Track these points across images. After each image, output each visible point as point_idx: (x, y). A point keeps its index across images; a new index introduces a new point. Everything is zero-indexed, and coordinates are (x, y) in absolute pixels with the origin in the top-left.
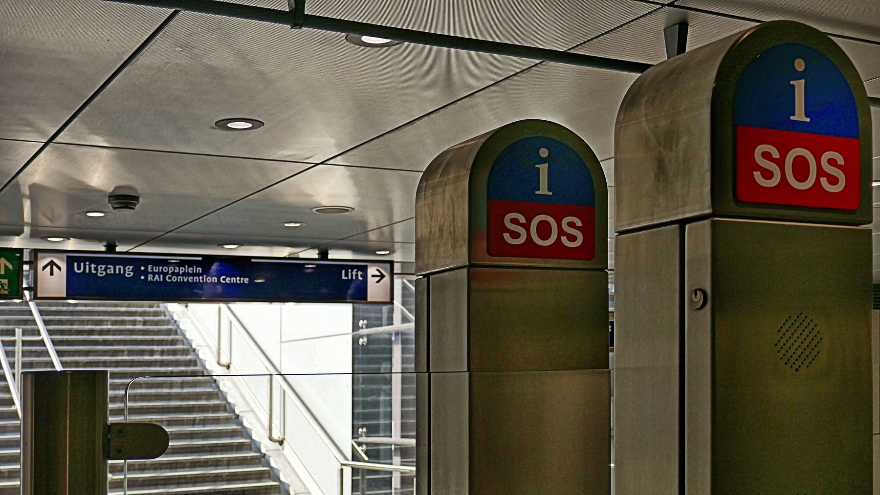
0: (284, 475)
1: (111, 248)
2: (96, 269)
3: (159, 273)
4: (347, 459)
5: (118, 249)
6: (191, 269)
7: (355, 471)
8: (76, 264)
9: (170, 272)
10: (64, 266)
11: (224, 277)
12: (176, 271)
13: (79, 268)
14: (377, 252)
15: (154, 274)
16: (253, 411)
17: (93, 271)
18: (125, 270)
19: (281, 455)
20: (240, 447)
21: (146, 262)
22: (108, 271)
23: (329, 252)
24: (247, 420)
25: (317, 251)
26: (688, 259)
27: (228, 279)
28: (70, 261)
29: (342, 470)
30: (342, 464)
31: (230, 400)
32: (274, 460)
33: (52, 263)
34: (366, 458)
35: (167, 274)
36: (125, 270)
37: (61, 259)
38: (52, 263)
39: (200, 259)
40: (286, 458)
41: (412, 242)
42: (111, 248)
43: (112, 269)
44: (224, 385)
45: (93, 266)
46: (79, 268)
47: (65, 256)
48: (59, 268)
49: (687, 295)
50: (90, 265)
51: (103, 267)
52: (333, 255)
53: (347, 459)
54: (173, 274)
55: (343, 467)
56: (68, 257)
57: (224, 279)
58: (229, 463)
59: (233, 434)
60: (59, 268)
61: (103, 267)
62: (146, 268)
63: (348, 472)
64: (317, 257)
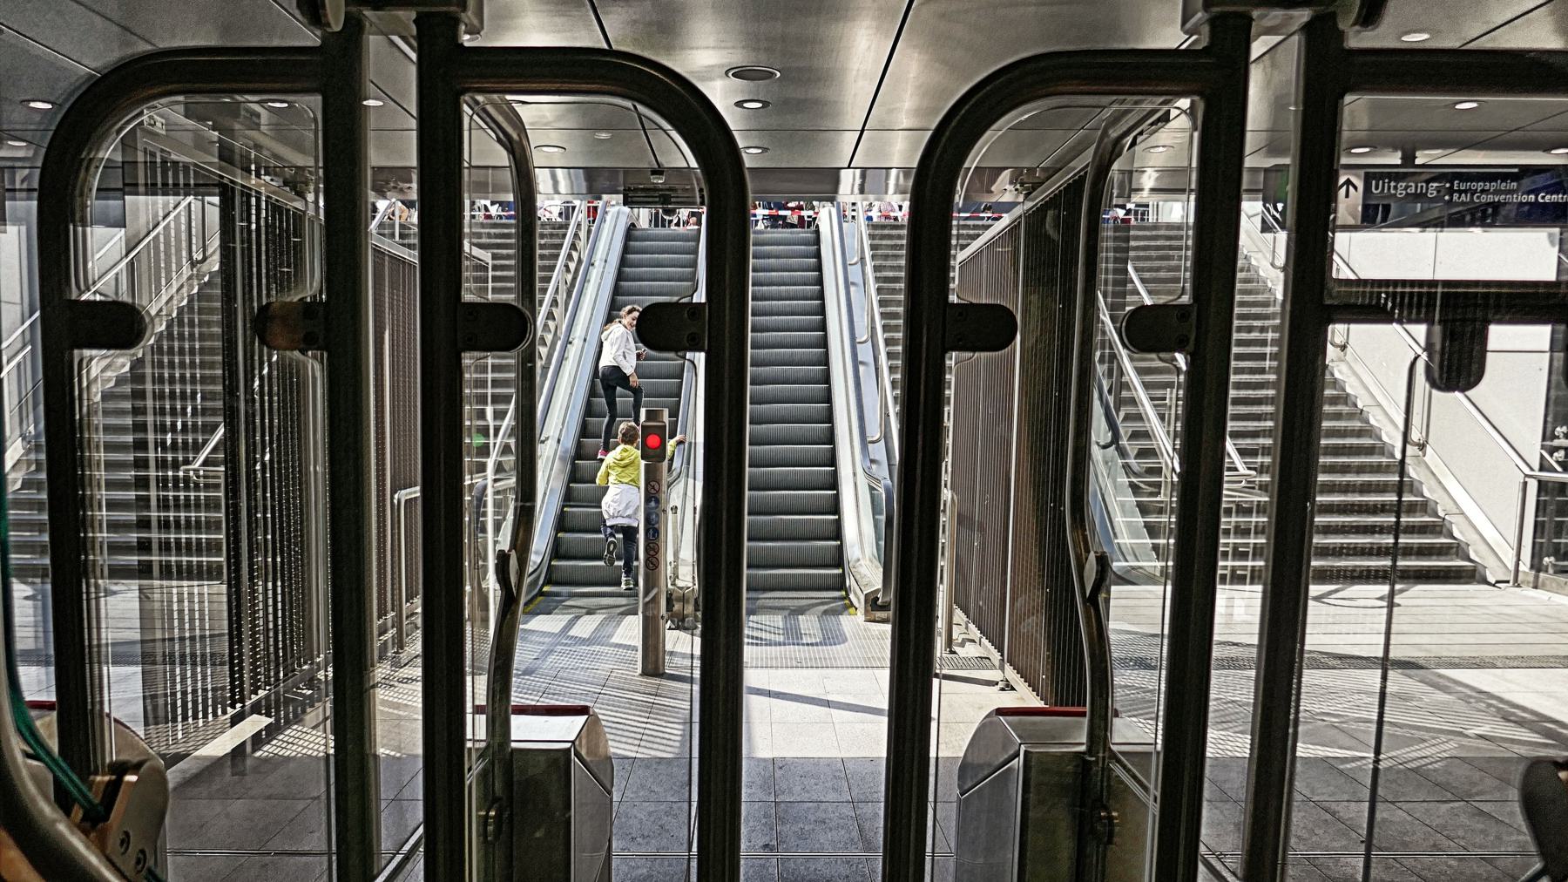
0: (1429, 490)
1: (1409, 159)
2: (1396, 188)
3: (1465, 192)
4: (1532, 469)
5: (1418, 161)
6: (1504, 184)
7: (1543, 486)
8: (1374, 182)
9: (1479, 189)
10: (1360, 184)
11: (1543, 194)
12: (1487, 188)
13: (1377, 188)
14: (1353, 151)
15: (1460, 192)
16: (1379, 405)
17: (1393, 192)
18: (1427, 189)
19: (1421, 462)
20: (1370, 451)
21: (1463, 177)
22: (1409, 191)
23: (1418, 154)
24: (1373, 416)
25: (1399, 154)
26: (936, 117)
27: (1548, 197)
28: (1368, 179)
29: (1525, 484)
30: (1526, 476)
31: (1348, 390)
32: (1414, 469)
33: (1348, 182)
34: (1559, 469)
35: (1476, 192)
36: (1427, 189)
37: (1357, 176)
38: (1348, 182)
39: (1516, 170)
40: (1428, 467)
41: (410, 127)
42: (1409, 159)
43: (1413, 188)
44: (1340, 372)
45: (1393, 184)
46: (1377, 188)
47: (1362, 172)
48: (1356, 188)
49: (779, 547)
50: (1389, 183)
51: (1404, 184)
52: (1396, 159)
53: (1532, 469)
54: (1483, 191)
55: (1527, 479)
56: (1366, 174)
57: (1543, 198)
58: (1361, 469)
59: (1359, 433)
60: (1356, 188)
61: (1404, 184)
62: (1452, 185)
63: (1533, 486)
64: (1399, 162)
